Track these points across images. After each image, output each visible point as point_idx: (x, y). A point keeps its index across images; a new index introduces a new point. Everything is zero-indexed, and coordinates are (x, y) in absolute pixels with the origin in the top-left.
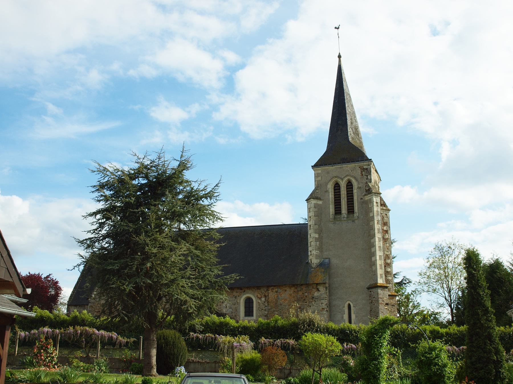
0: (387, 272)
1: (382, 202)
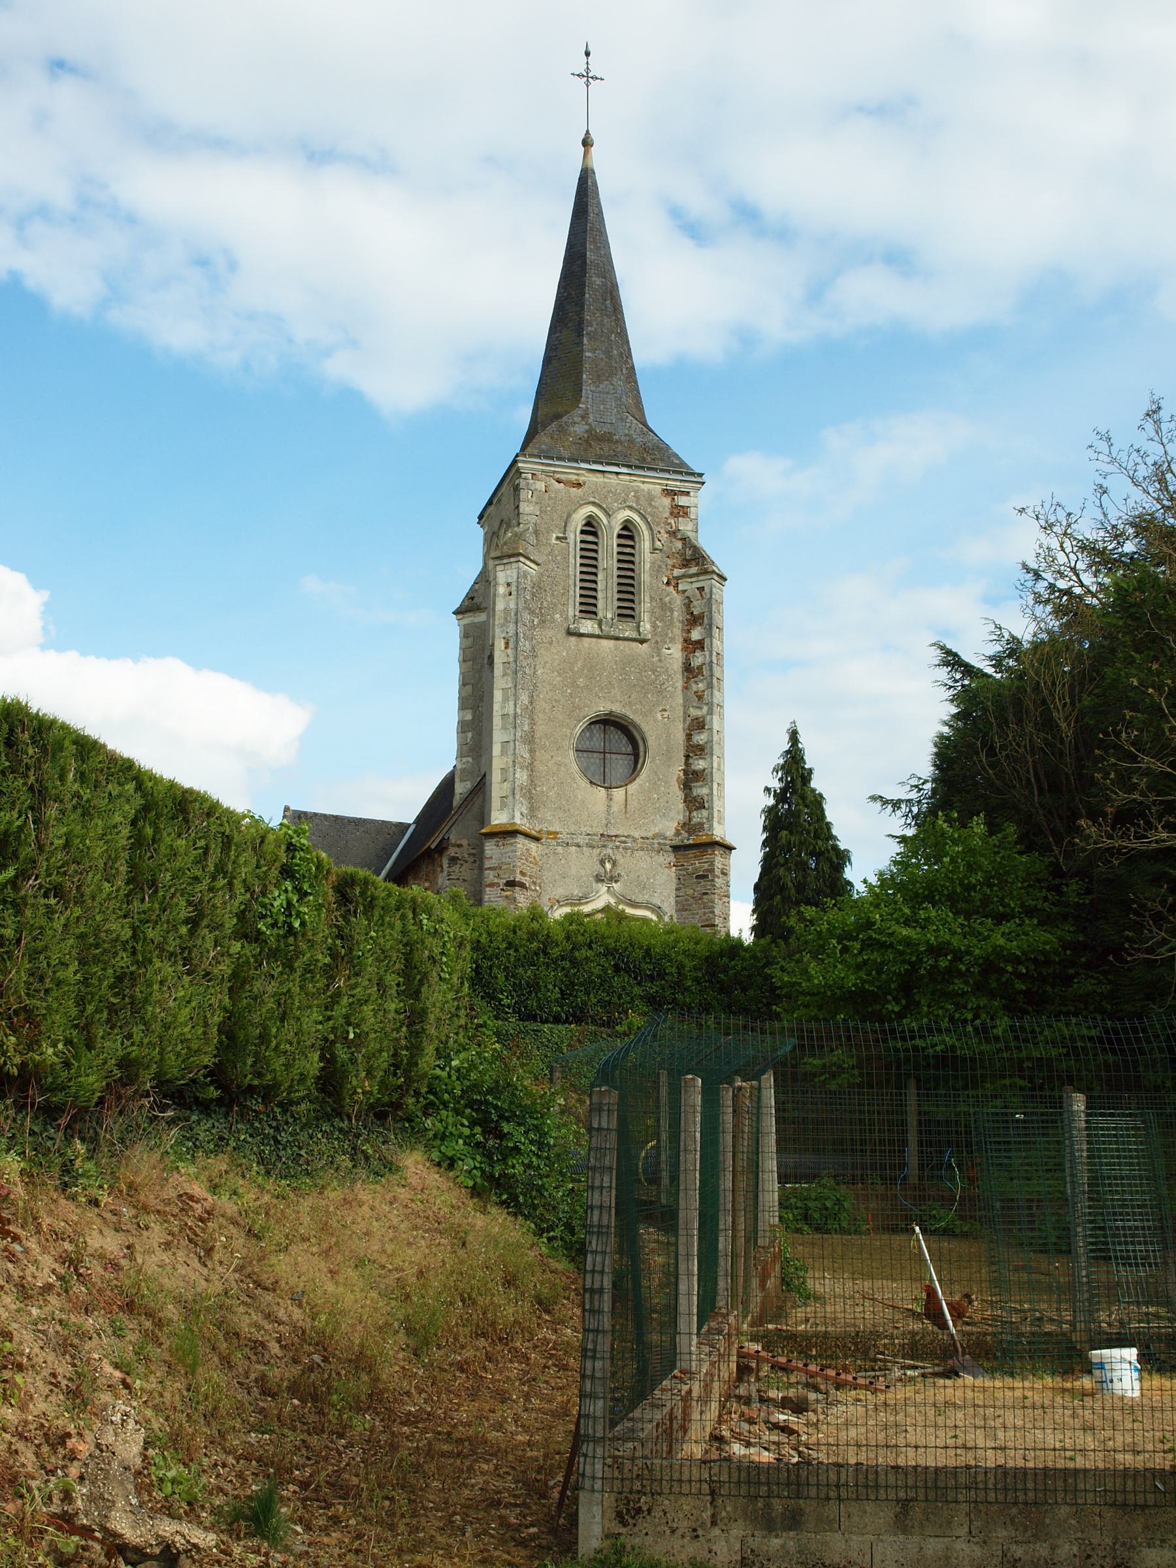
0: (695, 773)
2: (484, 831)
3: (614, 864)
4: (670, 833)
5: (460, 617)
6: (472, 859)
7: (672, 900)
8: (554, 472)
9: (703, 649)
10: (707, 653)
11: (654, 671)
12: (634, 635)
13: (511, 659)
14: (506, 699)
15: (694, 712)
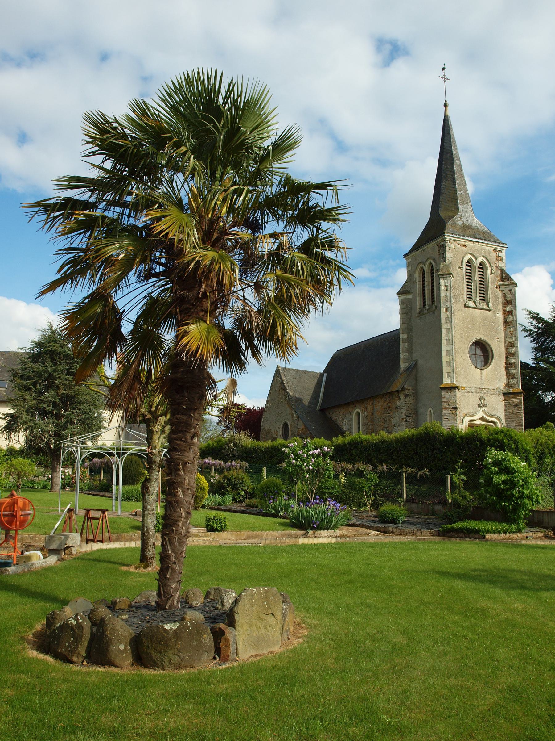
0: (511, 364)
1: (504, 275)
2: (441, 386)
3: (484, 399)
4: (502, 388)
9: (512, 314)
11: (494, 323)
12: (487, 308)
14: (448, 332)
15: (508, 340)
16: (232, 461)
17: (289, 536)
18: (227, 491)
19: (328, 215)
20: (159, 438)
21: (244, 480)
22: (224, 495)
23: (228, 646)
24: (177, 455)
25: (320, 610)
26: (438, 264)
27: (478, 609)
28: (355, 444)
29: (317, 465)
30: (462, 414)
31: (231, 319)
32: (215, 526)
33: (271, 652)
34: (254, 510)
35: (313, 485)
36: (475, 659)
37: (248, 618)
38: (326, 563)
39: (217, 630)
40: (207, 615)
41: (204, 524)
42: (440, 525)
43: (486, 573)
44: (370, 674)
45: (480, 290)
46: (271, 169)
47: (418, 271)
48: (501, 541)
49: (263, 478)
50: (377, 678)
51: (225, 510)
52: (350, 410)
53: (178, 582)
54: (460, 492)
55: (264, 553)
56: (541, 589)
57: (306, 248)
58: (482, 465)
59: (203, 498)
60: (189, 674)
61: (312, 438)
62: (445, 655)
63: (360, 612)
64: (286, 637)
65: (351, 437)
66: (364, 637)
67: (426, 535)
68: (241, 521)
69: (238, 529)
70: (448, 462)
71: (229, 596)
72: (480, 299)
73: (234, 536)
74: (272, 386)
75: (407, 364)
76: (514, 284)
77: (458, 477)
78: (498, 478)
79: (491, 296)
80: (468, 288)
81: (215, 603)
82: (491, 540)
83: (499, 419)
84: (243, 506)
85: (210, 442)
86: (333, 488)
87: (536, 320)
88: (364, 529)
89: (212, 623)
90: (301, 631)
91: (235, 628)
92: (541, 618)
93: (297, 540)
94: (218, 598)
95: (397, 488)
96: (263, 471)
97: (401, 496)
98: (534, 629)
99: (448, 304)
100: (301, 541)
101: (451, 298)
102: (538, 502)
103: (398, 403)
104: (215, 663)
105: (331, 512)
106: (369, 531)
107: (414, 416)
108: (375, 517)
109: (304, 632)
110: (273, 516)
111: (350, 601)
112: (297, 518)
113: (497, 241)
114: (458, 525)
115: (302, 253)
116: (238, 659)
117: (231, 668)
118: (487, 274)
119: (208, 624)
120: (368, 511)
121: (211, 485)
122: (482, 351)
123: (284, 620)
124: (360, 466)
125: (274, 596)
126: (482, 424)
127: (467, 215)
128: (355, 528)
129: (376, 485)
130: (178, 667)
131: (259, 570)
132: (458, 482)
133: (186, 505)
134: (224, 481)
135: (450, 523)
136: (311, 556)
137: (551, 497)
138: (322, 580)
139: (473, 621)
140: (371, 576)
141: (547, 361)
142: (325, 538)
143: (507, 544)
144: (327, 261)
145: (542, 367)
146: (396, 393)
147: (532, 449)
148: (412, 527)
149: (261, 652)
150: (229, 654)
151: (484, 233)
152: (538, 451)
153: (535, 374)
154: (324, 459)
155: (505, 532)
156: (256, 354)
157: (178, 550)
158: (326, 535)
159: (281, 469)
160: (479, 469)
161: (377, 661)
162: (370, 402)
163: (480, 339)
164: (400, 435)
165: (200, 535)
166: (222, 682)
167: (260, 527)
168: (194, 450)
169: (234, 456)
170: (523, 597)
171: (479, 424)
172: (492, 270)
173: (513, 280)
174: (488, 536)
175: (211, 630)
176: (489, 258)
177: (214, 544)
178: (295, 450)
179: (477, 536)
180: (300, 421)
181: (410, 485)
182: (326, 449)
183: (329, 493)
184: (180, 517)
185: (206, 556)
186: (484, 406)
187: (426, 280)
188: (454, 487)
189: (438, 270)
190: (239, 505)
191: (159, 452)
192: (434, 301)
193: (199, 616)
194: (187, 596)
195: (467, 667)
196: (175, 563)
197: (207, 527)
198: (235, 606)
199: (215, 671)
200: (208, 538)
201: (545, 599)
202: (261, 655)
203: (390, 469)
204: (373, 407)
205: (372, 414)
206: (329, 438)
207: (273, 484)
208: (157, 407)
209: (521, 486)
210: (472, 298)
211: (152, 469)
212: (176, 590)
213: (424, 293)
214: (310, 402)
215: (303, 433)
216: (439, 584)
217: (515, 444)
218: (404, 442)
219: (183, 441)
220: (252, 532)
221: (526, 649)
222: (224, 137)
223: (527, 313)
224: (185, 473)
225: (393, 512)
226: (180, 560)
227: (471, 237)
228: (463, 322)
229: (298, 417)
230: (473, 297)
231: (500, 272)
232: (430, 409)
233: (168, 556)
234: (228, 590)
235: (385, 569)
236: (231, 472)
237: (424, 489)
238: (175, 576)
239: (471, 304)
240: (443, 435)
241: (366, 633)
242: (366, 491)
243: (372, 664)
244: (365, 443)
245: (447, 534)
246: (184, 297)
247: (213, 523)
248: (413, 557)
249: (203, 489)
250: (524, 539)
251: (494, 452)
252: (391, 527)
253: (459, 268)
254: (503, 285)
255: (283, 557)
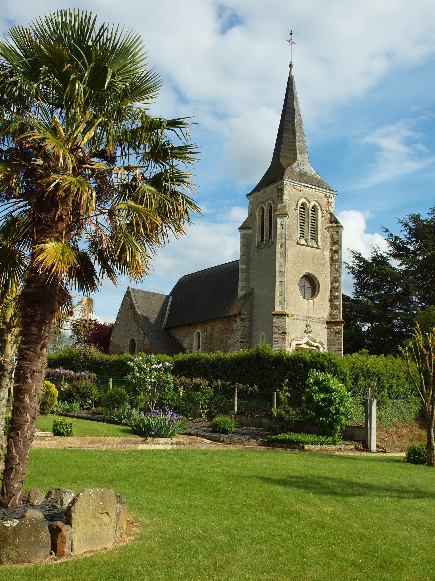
0: (334, 296)
1: (332, 219)
2: (273, 313)
4: (326, 317)
5: (241, 230)
6: (248, 319)
7: (326, 340)
8: (294, 185)
9: (337, 253)
10: (339, 255)
11: (322, 259)
12: (317, 246)
13: (283, 252)
16: (81, 371)
17: (130, 442)
18: (75, 399)
19: (181, 152)
20: (12, 347)
21: (91, 389)
22: (72, 402)
23: (64, 543)
24: (25, 364)
25: (152, 510)
26: (276, 205)
27: (293, 511)
28: (194, 361)
29: (158, 378)
30: (290, 338)
31: (88, 243)
32: (62, 430)
33: (104, 549)
34: (99, 417)
35: (155, 396)
36: (287, 556)
37: (84, 516)
38: (161, 467)
39: (55, 527)
40: (47, 513)
41: (51, 429)
42: (265, 436)
43: (302, 480)
44: (193, 569)
45: (311, 230)
46: (132, 108)
47: (258, 210)
48: (317, 451)
49: (109, 389)
50: (199, 572)
51: (73, 417)
52: (192, 330)
53: (20, 482)
54: (284, 407)
55: (105, 457)
56: (349, 495)
57: (156, 181)
58: (305, 384)
59: (52, 404)
60: (25, 569)
61: (156, 354)
62: (261, 552)
63: (188, 513)
64: (119, 535)
65: (191, 354)
66: (190, 536)
67: (253, 444)
68: (86, 426)
69: (83, 434)
70: (275, 380)
71: (68, 496)
72: (311, 238)
73: (79, 440)
74: (122, 305)
75: (244, 292)
76: (341, 227)
77: (284, 395)
78: (318, 396)
79: (320, 236)
80: (301, 228)
81: (56, 502)
82: (309, 451)
83: (322, 344)
84: (89, 414)
85: (62, 353)
86: (172, 400)
87: (358, 260)
88: (198, 438)
89: (51, 520)
90: (133, 529)
91: (71, 526)
92: (346, 520)
93: (137, 445)
94: (59, 498)
95: (230, 402)
96: (110, 381)
97: (233, 409)
98: (340, 530)
99: (283, 241)
100: (141, 447)
101: (285, 236)
102: (351, 419)
103: (235, 326)
104: (51, 559)
105: (169, 422)
106: (202, 439)
107: (248, 338)
108: (208, 427)
109: (136, 530)
110: (117, 423)
111: (180, 503)
112: (138, 426)
113: (328, 188)
114: (281, 436)
115: (152, 186)
116: (72, 554)
117: (65, 563)
118: (318, 217)
119: (46, 522)
120: (202, 422)
121: (61, 393)
122: (311, 284)
123: (118, 518)
124: (198, 381)
125: (110, 496)
126: (306, 348)
127: (303, 163)
128: (190, 437)
129: (211, 399)
130: (16, 562)
131: (100, 473)
132: (283, 398)
133: (32, 410)
134: (73, 389)
135: (274, 434)
136: (148, 460)
137: (363, 415)
138: (156, 482)
139: (288, 522)
140: (201, 480)
141: (365, 296)
142: (162, 444)
143: (323, 454)
144: (175, 194)
145: (361, 301)
146: (233, 317)
147: (348, 373)
148: (241, 437)
149: (95, 549)
150: (65, 550)
151: (317, 180)
152: (353, 374)
153: (355, 307)
154: (165, 373)
155: (322, 444)
156: (111, 273)
157: (23, 452)
158: (164, 442)
159: (126, 380)
160: (302, 387)
161: (200, 558)
162: (209, 324)
163: (309, 274)
164: (234, 355)
165: (47, 438)
166: (56, 576)
167: (103, 433)
168: (43, 360)
169: (84, 367)
170: (332, 501)
171: (304, 348)
172: (322, 213)
173: (340, 223)
174: (306, 447)
175: (49, 527)
176: (320, 202)
177: (59, 447)
178: (139, 363)
179: (297, 447)
180: (146, 338)
181: (241, 399)
182: (167, 364)
183: (169, 404)
184: (25, 421)
185: (51, 458)
186: (309, 332)
187: (265, 219)
188: (279, 403)
189: (276, 210)
190: (86, 412)
191: (11, 360)
192: (271, 237)
193: (39, 515)
194: (29, 495)
195: (280, 563)
196: (19, 464)
197: (54, 432)
198: (72, 505)
199: (51, 566)
200: (54, 442)
201: (351, 503)
202: (94, 551)
203: (224, 385)
204: (213, 328)
205: (211, 335)
206: (170, 354)
207: (118, 394)
208: (11, 319)
209: (337, 404)
210: (304, 237)
211: (4, 376)
212: (19, 489)
213: (263, 230)
214: (156, 321)
215: (148, 349)
216: (261, 489)
217: (334, 366)
218: (238, 362)
219: (32, 351)
220: (95, 437)
221: (332, 547)
222: (90, 75)
223: (351, 252)
224: (32, 381)
225: (225, 422)
226: (24, 461)
227: (306, 183)
228: (295, 257)
229: (144, 334)
230: (305, 236)
231: (329, 215)
232: (262, 332)
233: (12, 458)
234: (68, 490)
235: (213, 474)
236: (80, 382)
237: (253, 403)
238: (18, 477)
239: (303, 242)
240: (272, 357)
241: (193, 532)
242: (201, 403)
243: (195, 560)
244: (203, 361)
245: (271, 444)
246: (41, 219)
247: (60, 428)
248: (239, 464)
249: (53, 396)
250: (338, 451)
251: (315, 373)
252: (222, 437)
253: (295, 209)
254: (331, 227)
255: (122, 461)
